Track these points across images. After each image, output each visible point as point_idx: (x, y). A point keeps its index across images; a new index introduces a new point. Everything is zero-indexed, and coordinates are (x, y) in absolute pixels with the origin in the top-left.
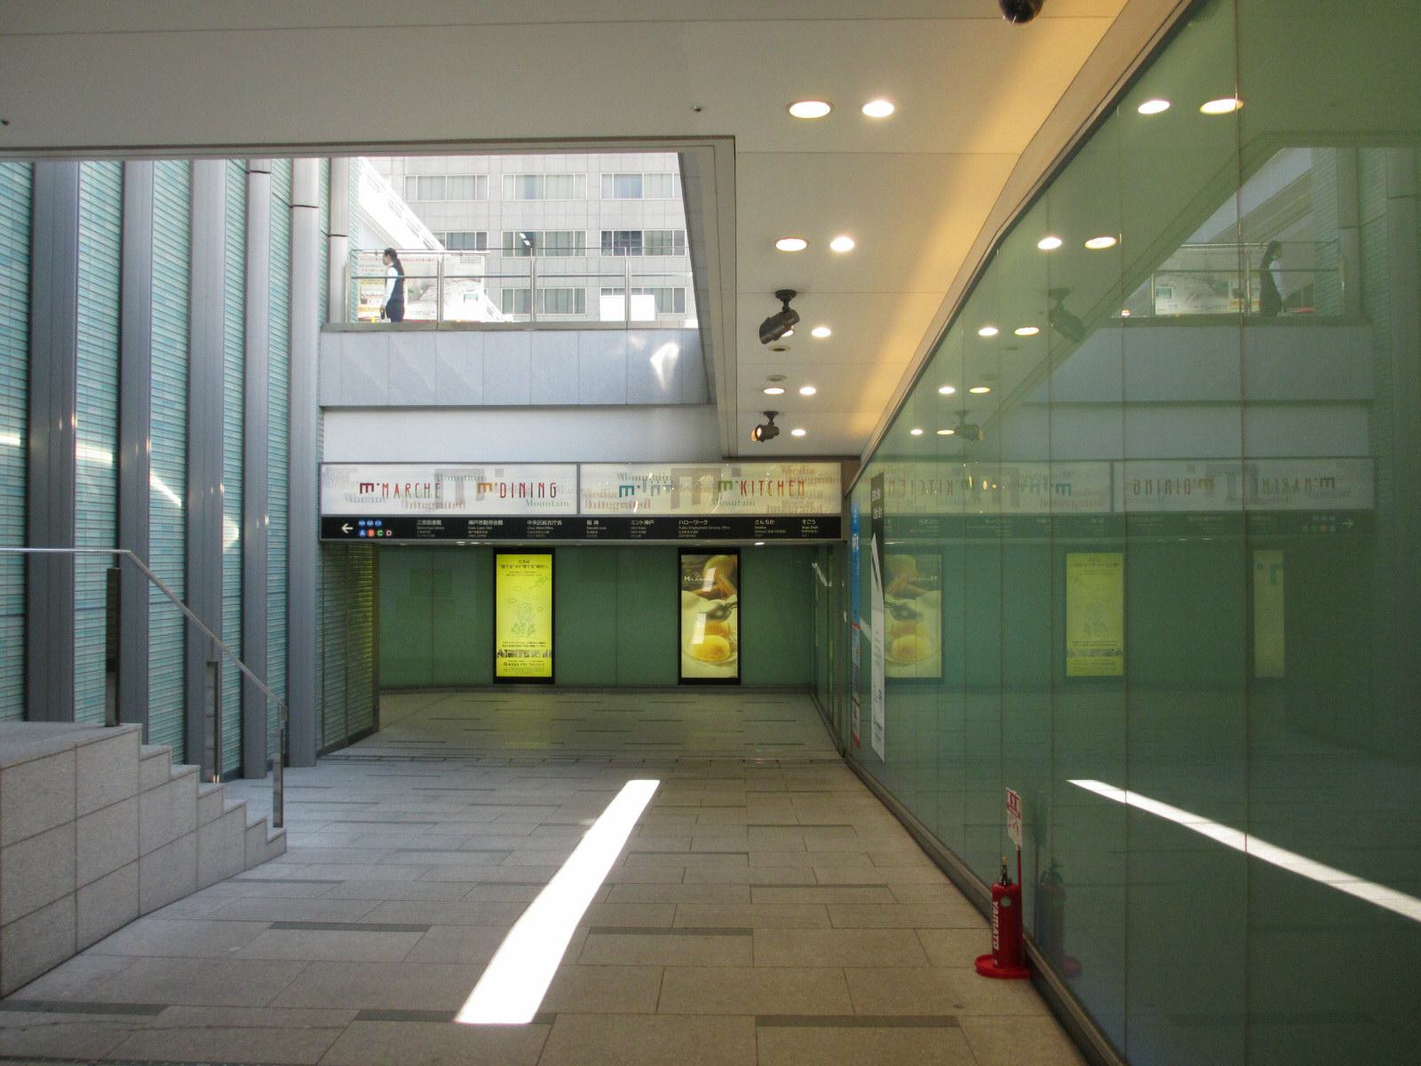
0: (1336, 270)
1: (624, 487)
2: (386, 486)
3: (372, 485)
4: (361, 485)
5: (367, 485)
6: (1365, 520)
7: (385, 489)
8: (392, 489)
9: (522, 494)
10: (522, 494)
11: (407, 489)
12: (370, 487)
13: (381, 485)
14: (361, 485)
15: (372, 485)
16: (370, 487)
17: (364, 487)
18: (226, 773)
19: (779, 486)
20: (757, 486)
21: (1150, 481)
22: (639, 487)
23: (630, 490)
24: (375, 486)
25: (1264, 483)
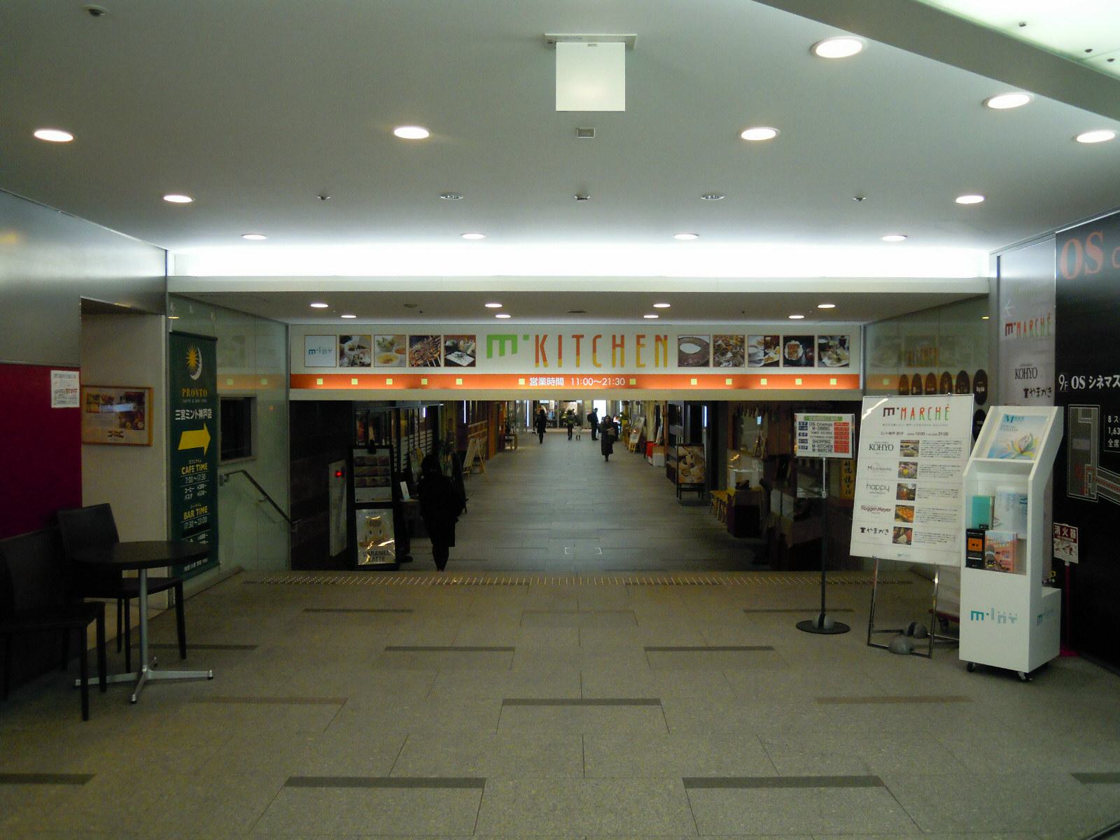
0: (1009, 552)
1: (975, 612)
2: (904, 410)
3: (982, 614)
4: (973, 612)
5: (978, 613)
6: (629, 46)
7: (903, 413)
8: (909, 412)
9: (903, 417)
10: (903, 417)
11: (921, 412)
12: (891, 411)
13: (900, 409)
14: (973, 612)
15: (982, 614)
16: (980, 616)
17: (887, 411)
18: (1045, 597)
19: (937, 411)
20: (884, 447)
21: (905, 409)
22: (988, 614)
23: (891, 411)
24: (896, 410)
25: (803, 443)
